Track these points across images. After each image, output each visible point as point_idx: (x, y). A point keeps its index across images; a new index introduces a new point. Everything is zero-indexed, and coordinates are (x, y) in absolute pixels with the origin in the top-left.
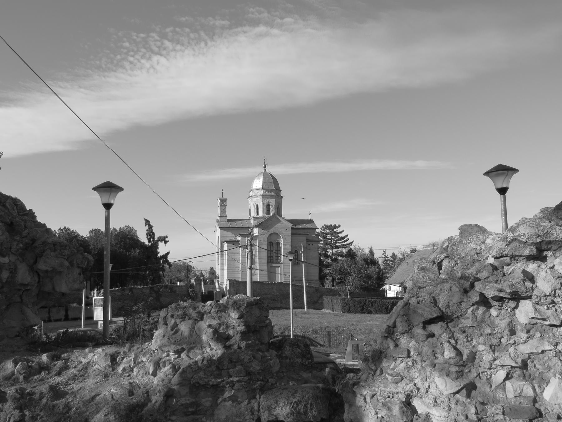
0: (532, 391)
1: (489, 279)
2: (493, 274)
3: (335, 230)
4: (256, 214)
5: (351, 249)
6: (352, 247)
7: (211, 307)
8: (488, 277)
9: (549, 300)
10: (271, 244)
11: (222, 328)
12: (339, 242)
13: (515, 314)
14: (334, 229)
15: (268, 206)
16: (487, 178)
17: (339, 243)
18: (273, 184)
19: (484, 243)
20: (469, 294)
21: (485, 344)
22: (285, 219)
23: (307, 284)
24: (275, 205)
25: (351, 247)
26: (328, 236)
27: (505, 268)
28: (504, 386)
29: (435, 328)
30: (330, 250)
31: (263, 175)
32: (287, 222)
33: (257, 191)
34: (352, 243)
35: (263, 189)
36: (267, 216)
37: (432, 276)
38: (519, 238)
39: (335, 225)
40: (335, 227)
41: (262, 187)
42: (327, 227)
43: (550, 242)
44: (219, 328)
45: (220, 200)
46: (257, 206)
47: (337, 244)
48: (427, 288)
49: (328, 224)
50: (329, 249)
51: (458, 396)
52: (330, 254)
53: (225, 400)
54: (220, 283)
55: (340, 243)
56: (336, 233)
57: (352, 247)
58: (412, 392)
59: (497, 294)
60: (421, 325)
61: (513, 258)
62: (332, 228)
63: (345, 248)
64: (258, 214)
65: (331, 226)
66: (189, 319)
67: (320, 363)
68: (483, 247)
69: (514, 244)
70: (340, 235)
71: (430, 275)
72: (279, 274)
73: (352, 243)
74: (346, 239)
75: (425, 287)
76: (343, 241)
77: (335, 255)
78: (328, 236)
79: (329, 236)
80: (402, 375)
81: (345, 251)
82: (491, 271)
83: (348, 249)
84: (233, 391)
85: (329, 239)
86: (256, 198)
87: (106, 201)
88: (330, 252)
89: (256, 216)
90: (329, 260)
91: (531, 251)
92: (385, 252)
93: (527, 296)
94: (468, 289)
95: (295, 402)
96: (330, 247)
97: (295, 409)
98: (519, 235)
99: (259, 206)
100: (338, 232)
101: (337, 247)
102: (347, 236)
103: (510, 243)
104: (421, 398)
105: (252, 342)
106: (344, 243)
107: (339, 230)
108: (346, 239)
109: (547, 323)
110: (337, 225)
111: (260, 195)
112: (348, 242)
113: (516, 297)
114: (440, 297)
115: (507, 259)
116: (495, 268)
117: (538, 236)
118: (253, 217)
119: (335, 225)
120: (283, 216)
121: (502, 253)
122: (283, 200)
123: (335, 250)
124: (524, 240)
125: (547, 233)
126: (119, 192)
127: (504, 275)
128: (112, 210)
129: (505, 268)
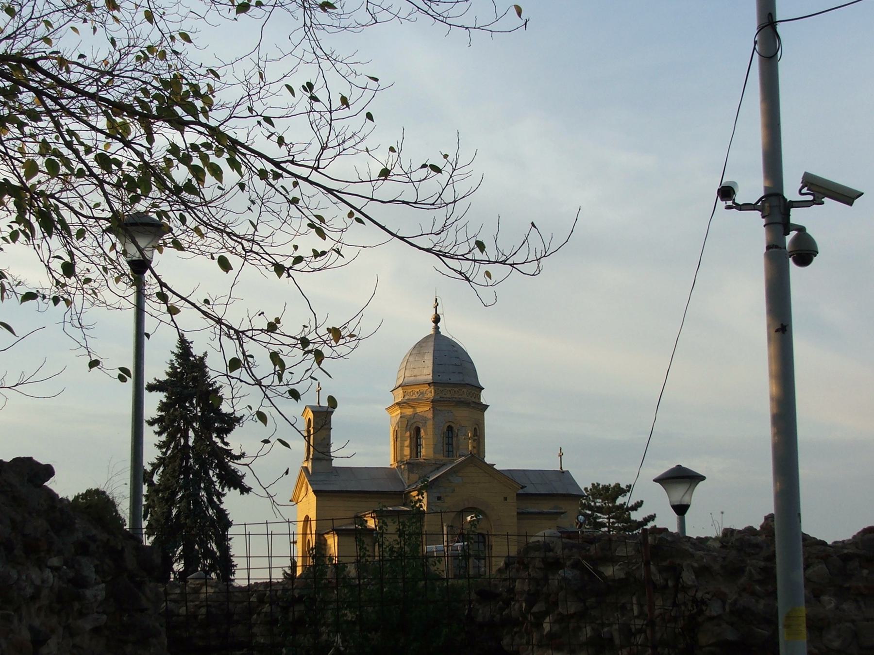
0: (728, 638)
3: (620, 501)
10: (481, 538)
16: (863, 192)
26: (600, 517)
35: (434, 383)
39: (618, 485)
40: (618, 491)
41: (430, 377)
65: (606, 488)
67: (330, 412)
72: (129, 123)
78: (600, 517)
79: (603, 519)
85: (603, 525)
105: (362, 529)
110: (623, 486)
119: (618, 485)
122: (487, 414)
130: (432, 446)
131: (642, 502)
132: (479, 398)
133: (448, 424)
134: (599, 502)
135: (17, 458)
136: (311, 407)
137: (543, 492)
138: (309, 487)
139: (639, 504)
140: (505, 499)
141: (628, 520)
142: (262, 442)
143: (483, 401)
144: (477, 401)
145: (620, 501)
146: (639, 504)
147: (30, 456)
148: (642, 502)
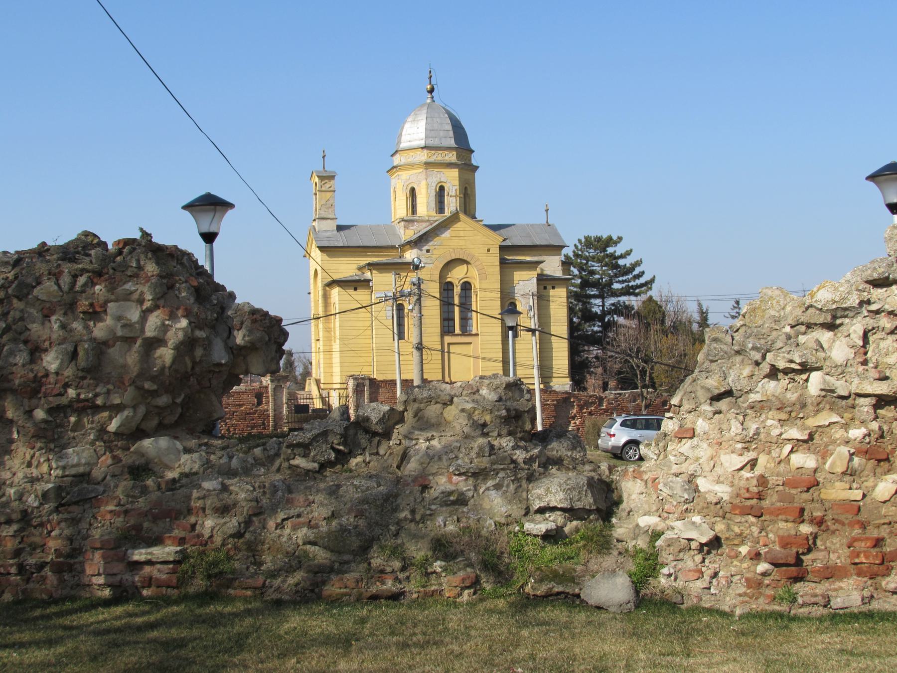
1: (783, 350)
2: (786, 344)
3: (610, 250)
4: (410, 211)
5: (650, 299)
6: (654, 293)
7: (461, 389)
8: (782, 348)
9: (840, 370)
11: (477, 412)
12: (621, 279)
13: (807, 387)
14: (608, 246)
15: (441, 192)
17: (619, 282)
18: (451, 134)
19: (783, 309)
20: (761, 366)
21: (773, 419)
22: (484, 223)
23: (542, 386)
24: (458, 187)
25: (649, 293)
26: (593, 266)
27: (800, 337)
28: (789, 460)
29: (723, 404)
30: (598, 301)
31: (425, 111)
32: (487, 229)
33: (412, 153)
34: (652, 281)
36: (440, 218)
37: (725, 347)
38: (815, 304)
40: (609, 242)
42: (589, 243)
43: (846, 309)
44: (473, 413)
45: (318, 176)
46: (413, 190)
47: (616, 286)
48: (719, 361)
49: (593, 234)
50: (595, 297)
51: (743, 472)
52: (597, 310)
53: (488, 489)
54: (322, 386)
55: (623, 282)
56: (613, 256)
57: (654, 293)
58: (696, 471)
59: (788, 365)
60: (709, 401)
61: (809, 326)
62: (602, 243)
63: (636, 295)
64: (414, 210)
65: (599, 239)
66: (436, 403)
68: (782, 314)
69: (811, 310)
70: (621, 262)
71: (722, 347)
73: (652, 281)
74: (636, 272)
75: (717, 361)
76: (630, 276)
77: (610, 312)
78: (593, 266)
79: (596, 267)
80: (686, 454)
81: (634, 302)
82: (785, 341)
83: (644, 297)
84: (498, 479)
86: (409, 170)
87: (205, 229)
88: (596, 306)
89: (410, 217)
90: (594, 325)
91: (825, 318)
92: (738, 303)
93: (818, 367)
94: (760, 361)
95: (569, 489)
96: (597, 293)
97: (569, 495)
98: (816, 301)
99: (417, 191)
100: (618, 254)
101: (615, 294)
102: (638, 263)
103: (807, 309)
104: (705, 477)
106: (632, 283)
107: (619, 250)
108: (636, 272)
109: (835, 395)
110: (615, 238)
111: (420, 164)
112: (642, 280)
113: (806, 368)
114: (731, 371)
115: (803, 328)
116: (789, 337)
117: (835, 302)
118: (403, 220)
120: (479, 218)
121: (798, 321)
122: (477, 174)
123: (610, 301)
124: (820, 307)
125: (844, 299)
126: (227, 211)
127: (798, 345)
128: (216, 243)
129: (800, 337)
130: (425, 204)
131: (631, 251)
132: (470, 160)
133: (440, 185)
134: (592, 252)
135: (466, 135)
136: (317, 172)
137: (538, 244)
138: (314, 242)
139: (628, 253)
140: (489, 250)
141: (617, 266)
142: (141, 230)
143: (474, 162)
144: (467, 162)
145: (610, 250)
146: (628, 253)
147: (203, 193)
148: (631, 251)
